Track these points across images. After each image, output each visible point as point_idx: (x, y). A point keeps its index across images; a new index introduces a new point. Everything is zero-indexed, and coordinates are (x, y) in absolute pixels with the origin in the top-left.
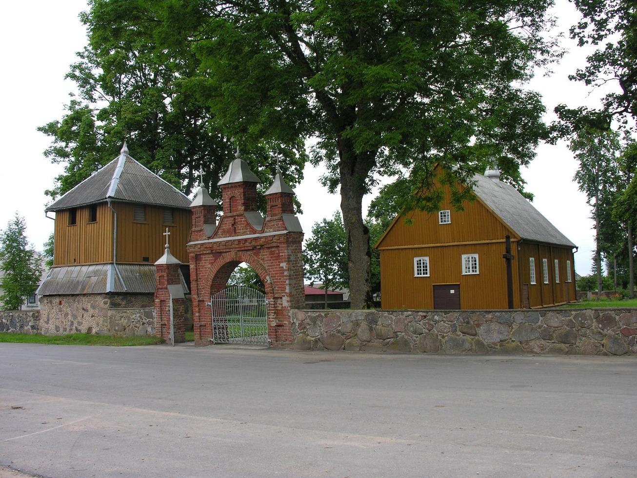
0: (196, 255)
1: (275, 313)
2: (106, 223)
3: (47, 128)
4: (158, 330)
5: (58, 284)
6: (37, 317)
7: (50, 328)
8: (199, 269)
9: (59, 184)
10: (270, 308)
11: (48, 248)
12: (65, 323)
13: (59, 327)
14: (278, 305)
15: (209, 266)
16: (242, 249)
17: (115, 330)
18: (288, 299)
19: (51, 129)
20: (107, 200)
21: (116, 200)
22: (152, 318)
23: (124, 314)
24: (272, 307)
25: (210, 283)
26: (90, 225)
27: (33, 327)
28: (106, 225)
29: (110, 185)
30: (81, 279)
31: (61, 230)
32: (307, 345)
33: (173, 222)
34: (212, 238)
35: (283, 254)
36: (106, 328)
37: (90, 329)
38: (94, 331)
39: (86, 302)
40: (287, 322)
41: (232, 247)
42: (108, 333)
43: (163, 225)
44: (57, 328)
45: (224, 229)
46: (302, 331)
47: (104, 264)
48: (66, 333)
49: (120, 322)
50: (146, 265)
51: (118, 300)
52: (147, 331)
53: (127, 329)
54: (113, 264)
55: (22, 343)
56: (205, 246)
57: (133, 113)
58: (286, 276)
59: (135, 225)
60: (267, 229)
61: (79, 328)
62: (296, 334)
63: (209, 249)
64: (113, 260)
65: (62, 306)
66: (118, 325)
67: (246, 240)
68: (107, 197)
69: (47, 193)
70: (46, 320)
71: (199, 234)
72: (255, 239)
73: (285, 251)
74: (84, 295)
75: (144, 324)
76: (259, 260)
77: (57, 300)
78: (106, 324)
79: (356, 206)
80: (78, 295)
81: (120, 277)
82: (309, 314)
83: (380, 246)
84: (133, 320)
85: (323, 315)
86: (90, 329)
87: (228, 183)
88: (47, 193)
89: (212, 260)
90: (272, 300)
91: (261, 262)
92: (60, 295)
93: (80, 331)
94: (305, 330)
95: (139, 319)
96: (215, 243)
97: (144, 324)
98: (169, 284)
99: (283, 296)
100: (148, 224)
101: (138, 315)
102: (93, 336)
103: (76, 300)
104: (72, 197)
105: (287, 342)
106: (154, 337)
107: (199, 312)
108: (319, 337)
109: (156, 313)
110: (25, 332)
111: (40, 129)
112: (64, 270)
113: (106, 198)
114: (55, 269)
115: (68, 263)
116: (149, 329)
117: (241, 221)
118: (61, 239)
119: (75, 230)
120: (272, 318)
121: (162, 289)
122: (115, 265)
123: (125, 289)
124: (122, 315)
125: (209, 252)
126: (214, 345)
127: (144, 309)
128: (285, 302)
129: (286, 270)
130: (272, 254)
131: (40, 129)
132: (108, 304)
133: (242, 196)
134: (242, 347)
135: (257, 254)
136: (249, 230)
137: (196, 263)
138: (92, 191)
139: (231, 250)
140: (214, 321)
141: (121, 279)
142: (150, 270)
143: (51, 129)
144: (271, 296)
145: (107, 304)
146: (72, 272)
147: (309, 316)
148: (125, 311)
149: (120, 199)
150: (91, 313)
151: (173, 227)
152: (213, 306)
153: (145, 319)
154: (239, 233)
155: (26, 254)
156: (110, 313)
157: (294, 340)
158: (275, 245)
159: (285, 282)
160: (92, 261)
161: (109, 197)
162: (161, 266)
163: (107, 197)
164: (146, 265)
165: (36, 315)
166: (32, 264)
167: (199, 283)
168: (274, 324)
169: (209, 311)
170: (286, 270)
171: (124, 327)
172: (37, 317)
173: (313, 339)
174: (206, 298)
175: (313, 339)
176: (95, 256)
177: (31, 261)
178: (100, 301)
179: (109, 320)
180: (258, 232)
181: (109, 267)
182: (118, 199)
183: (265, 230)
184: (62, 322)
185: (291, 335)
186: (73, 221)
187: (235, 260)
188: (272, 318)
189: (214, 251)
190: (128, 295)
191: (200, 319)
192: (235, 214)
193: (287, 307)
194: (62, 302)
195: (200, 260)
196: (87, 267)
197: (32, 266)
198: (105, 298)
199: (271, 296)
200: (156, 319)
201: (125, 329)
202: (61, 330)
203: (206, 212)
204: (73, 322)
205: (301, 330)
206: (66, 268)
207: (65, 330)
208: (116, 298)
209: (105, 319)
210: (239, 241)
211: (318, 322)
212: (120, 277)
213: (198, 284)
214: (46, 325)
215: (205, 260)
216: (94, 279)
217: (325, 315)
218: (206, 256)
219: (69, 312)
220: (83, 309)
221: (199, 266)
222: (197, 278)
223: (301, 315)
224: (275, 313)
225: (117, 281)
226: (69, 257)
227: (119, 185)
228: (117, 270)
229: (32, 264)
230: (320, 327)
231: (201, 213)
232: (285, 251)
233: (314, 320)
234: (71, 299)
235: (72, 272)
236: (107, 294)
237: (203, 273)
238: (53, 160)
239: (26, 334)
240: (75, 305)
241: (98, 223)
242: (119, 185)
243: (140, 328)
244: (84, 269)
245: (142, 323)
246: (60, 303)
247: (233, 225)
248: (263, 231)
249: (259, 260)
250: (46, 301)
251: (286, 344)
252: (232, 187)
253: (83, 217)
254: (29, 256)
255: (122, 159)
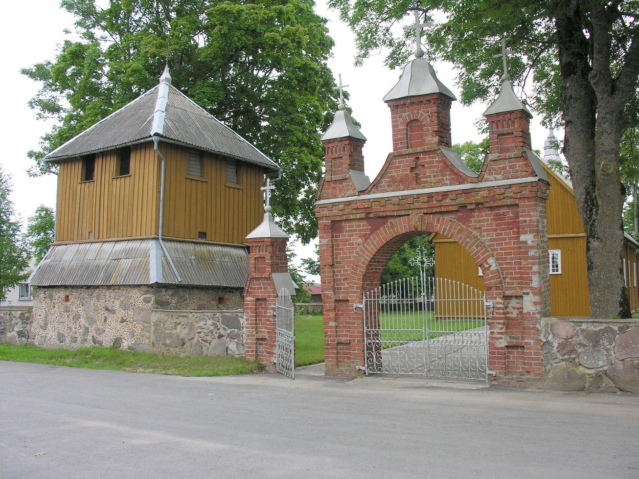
0: (333, 221)
1: (504, 324)
2: (146, 175)
3: (34, 71)
4: (249, 347)
5: (63, 269)
6: (28, 318)
7: (49, 336)
8: (338, 245)
9: (47, 144)
10: (495, 315)
11: (34, 224)
12: (73, 329)
13: (64, 336)
14: (510, 309)
15: (360, 241)
16: (435, 210)
17: (165, 344)
18: (537, 299)
19: (39, 73)
20: (154, 138)
21: (167, 140)
22: (239, 327)
23: (181, 319)
24: (500, 314)
25: (362, 270)
26: (119, 180)
27: (21, 334)
28: (146, 180)
29: (152, 120)
30: (103, 262)
31: (68, 190)
32: (577, 383)
33: (237, 183)
34: (368, 193)
35: (528, 219)
36: (147, 341)
37: (117, 342)
38: (125, 344)
39: (111, 299)
40: (532, 342)
41: (412, 207)
42: (152, 348)
43: (225, 186)
44: (61, 337)
45: (392, 177)
46: (566, 357)
47: (143, 239)
48: (77, 345)
49: (174, 332)
50: (202, 243)
51: (166, 295)
52: (227, 349)
53: (188, 345)
54: (157, 239)
55: (7, 360)
56: (354, 206)
57: (157, 47)
58: (533, 258)
59: (189, 182)
60: (489, 174)
61: (99, 338)
62: (552, 362)
63: (363, 210)
64: (157, 233)
65: (69, 304)
66: (170, 336)
67: (445, 194)
68: (152, 134)
69: (31, 155)
70: (42, 323)
71: (338, 185)
72: (466, 192)
73: (532, 213)
74: (109, 287)
75: (220, 336)
76: (470, 230)
77: (62, 294)
78: (147, 334)
79: (614, 147)
80: (97, 287)
81: (171, 261)
82: (584, 326)
83: (435, 238)
84: (200, 330)
85: (615, 328)
86: (117, 342)
87: (408, 96)
88: (31, 155)
89: (365, 230)
90: (499, 300)
91: (475, 233)
92: (65, 287)
93: (100, 343)
94: (573, 356)
95: (212, 328)
96: (376, 200)
97: (220, 336)
98: (273, 271)
99: (524, 293)
100: (207, 182)
101: (210, 322)
102: (123, 352)
103: (95, 295)
104: (88, 141)
105: (531, 376)
106: (242, 360)
107: (336, 320)
108: (605, 368)
109: (247, 320)
110: (8, 341)
111: (24, 72)
112: (72, 249)
113: (150, 136)
114: (58, 248)
115: (80, 237)
116: (232, 346)
117: (432, 162)
118: (67, 202)
119: (92, 190)
120: (499, 333)
121: (258, 279)
122: (161, 241)
123: (178, 280)
124: (177, 321)
125: (363, 215)
126: (366, 378)
127: (221, 313)
128: (529, 304)
129: (532, 247)
130: (499, 219)
131: (24, 72)
132: (152, 303)
133: (435, 118)
134: (435, 384)
135: (465, 220)
136: (448, 177)
137: (332, 237)
138: (123, 130)
139: (410, 212)
140: (368, 336)
141: (172, 264)
142: (209, 251)
143: (39, 73)
144: (499, 294)
145: (149, 302)
146: (86, 252)
147: (582, 330)
148: (185, 314)
149: (171, 139)
150: (120, 317)
151: (239, 189)
152: (367, 309)
153: (224, 329)
154: (425, 182)
155: (9, 227)
156: (154, 317)
157: (546, 372)
158: (509, 202)
159: (531, 268)
160: (120, 235)
161: (156, 134)
162: (261, 240)
163: (152, 134)
164: (202, 243)
165: (27, 315)
166: (18, 241)
167: (336, 270)
168: (502, 343)
169: (357, 319)
170: (532, 247)
171: (182, 339)
172: (28, 318)
173: (592, 372)
174: (353, 296)
175: (592, 372)
176: (125, 228)
177: (16, 237)
178: (138, 297)
179: (152, 329)
180: (469, 180)
181: (152, 244)
182: (168, 138)
183: (486, 176)
184: (70, 328)
185: (541, 365)
186: (88, 176)
187: (419, 229)
188: (499, 333)
189: (371, 215)
190: (181, 289)
191: (337, 332)
192: (419, 149)
193: (534, 314)
194: (70, 297)
195: (340, 229)
196: (112, 244)
197: (19, 243)
198: (147, 292)
199: (499, 294)
200: (245, 330)
201: (184, 344)
202: (68, 340)
203: (352, 150)
204: (88, 329)
205: (564, 355)
206: (75, 247)
207: (74, 340)
208: (164, 293)
209: (146, 325)
210: (430, 196)
211: (605, 342)
212: (171, 261)
213: (334, 272)
214: (41, 332)
215: (350, 231)
216: (126, 263)
217: (621, 329)
218: (354, 223)
219: (82, 313)
220: (107, 309)
221: (336, 241)
222: (333, 262)
223: (564, 328)
224: (504, 324)
225: (166, 266)
226: (80, 228)
227: (166, 120)
228: (165, 249)
229: (18, 241)
230: (607, 350)
231: (344, 151)
232: (532, 213)
233: (595, 339)
234: (85, 294)
235: (86, 252)
236: (151, 286)
237: (346, 253)
238: (38, 116)
239: (9, 344)
240: (92, 302)
241: (132, 178)
242: (166, 120)
243: (213, 344)
244: (108, 247)
245: (217, 335)
246: (67, 299)
247: (412, 169)
248: (479, 179)
249: (470, 230)
250: (42, 295)
251: (527, 380)
252: (412, 104)
253: (105, 169)
254: (14, 230)
255: (163, 88)
